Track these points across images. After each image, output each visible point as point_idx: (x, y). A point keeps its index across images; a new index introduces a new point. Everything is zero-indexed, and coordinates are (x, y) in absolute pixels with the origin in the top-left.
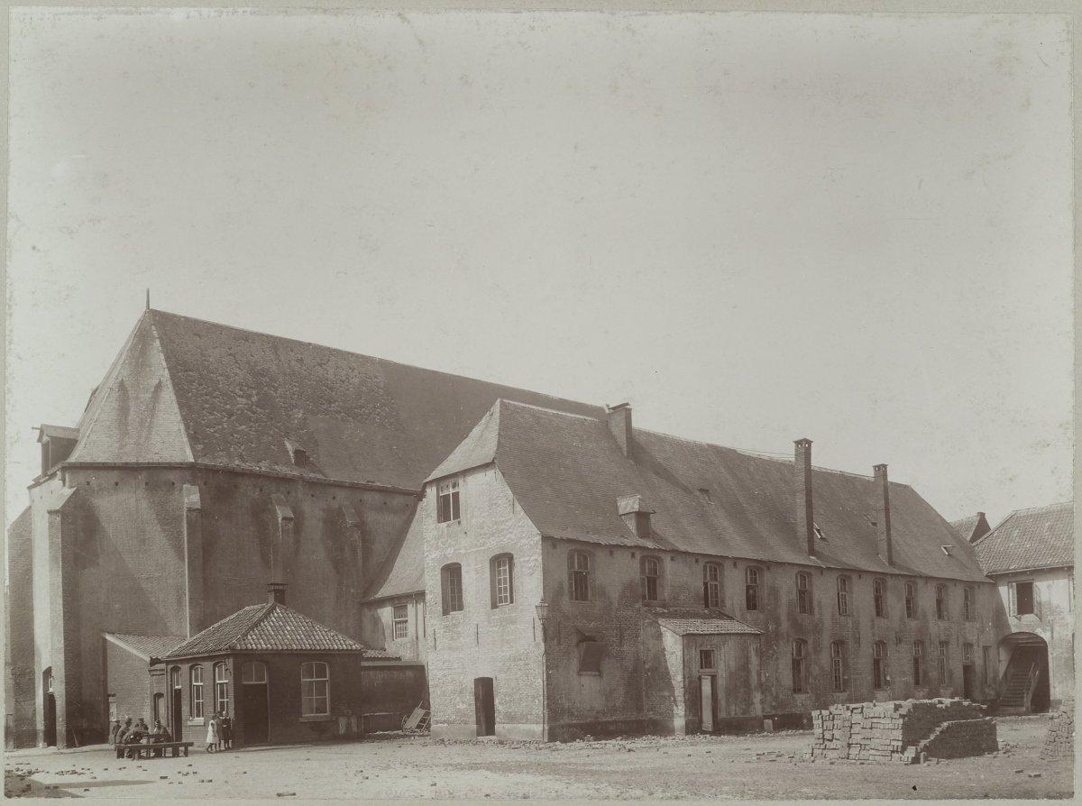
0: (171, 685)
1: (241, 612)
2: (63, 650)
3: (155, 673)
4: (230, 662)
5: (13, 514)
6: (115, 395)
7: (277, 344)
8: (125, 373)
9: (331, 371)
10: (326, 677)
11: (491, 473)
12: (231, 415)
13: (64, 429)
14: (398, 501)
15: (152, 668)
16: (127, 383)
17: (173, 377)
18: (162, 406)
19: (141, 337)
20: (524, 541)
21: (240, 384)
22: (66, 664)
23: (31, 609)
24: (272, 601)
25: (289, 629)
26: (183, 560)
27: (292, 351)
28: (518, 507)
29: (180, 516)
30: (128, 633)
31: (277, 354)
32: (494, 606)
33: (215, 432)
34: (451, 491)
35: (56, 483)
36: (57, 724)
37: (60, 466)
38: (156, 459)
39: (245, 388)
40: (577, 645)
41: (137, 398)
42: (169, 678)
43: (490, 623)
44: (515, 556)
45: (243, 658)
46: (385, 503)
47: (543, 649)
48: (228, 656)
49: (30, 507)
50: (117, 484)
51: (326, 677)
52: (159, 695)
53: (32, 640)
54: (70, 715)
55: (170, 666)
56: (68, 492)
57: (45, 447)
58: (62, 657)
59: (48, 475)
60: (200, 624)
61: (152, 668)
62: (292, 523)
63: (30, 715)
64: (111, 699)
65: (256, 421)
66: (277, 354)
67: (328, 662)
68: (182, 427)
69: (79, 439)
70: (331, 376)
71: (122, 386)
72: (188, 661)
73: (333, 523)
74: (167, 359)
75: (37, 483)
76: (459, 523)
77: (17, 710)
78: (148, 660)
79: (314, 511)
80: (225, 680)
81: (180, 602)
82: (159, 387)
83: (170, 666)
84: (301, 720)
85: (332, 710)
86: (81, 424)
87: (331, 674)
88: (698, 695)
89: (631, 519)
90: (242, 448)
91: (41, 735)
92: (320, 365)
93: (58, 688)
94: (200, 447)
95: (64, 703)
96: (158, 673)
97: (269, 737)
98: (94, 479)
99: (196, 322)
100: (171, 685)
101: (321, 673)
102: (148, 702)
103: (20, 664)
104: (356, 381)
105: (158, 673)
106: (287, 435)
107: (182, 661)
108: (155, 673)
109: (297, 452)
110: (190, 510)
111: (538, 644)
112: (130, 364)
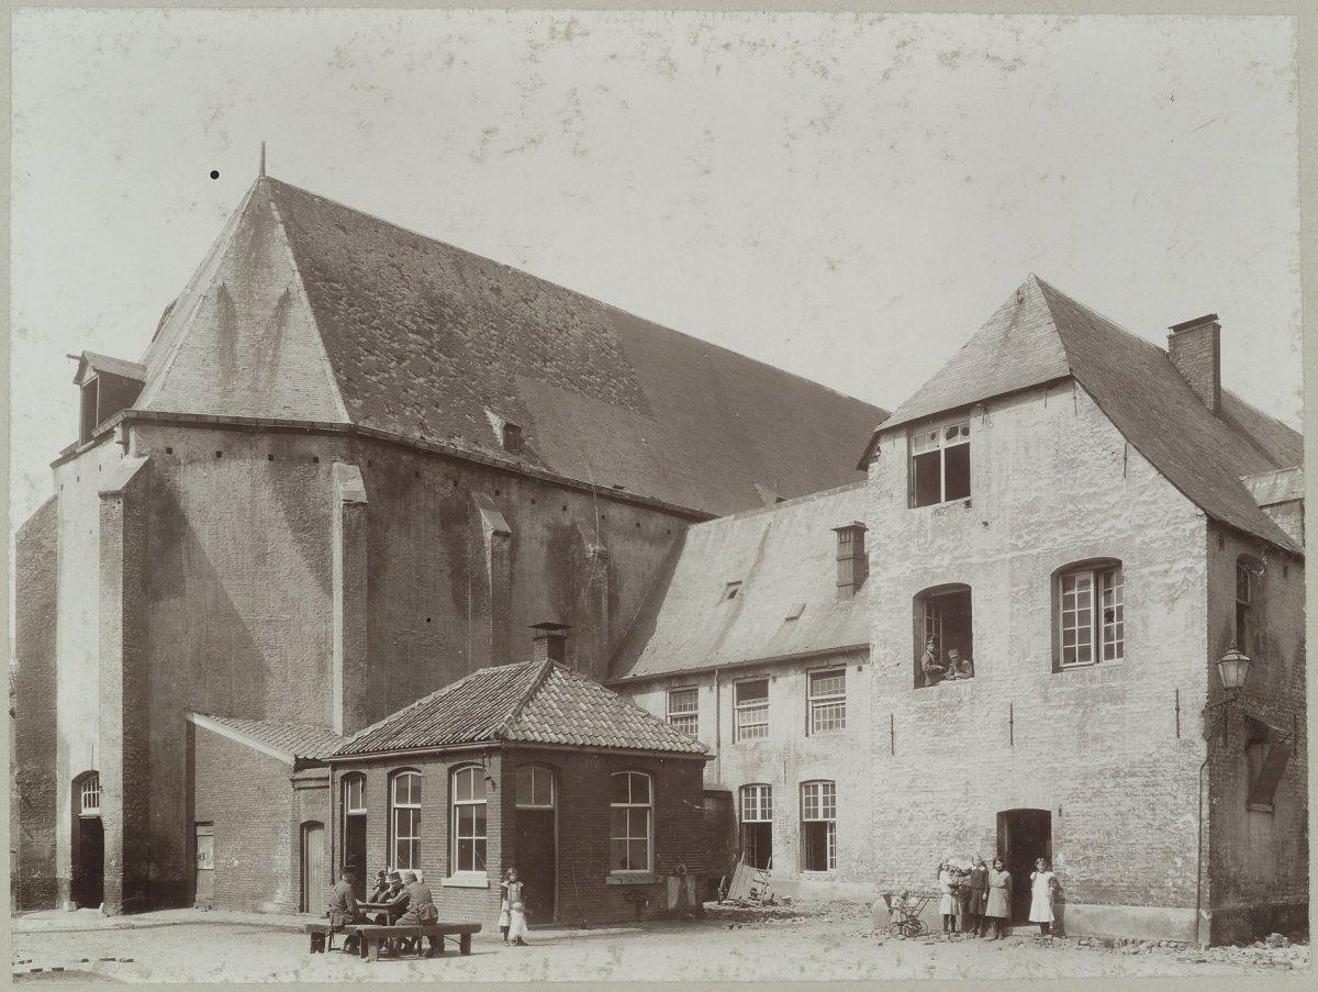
0: (342, 807)
1: (471, 677)
2: (120, 740)
3: (302, 784)
4: (494, 767)
5: (21, 514)
6: (211, 309)
7: (461, 261)
8: (228, 273)
9: (541, 314)
10: (647, 802)
11: (1060, 401)
12: (401, 359)
13: (123, 363)
14: (657, 522)
15: (298, 776)
16: (231, 289)
17: (308, 287)
18: (291, 331)
19: (254, 218)
20: (1151, 533)
21: (412, 312)
22: (125, 766)
23: (52, 671)
24: (541, 663)
25: (585, 707)
26: (327, 588)
27: (483, 273)
28: (1139, 463)
29: (328, 517)
30: (230, 716)
31: (461, 276)
32: (1056, 669)
33: (379, 382)
34: (943, 444)
35: (112, 448)
36: (106, 870)
37: (120, 417)
38: (286, 415)
39: (420, 320)
40: (1247, 749)
41: (250, 316)
42: (338, 793)
43: (1047, 699)
44: (1125, 564)
45: (521, 757)
46: (638, 525)
47: (1204, 754)
48: (490, 751)
49: (56, 498)
50: (219, 454)
51: (647, 802)
52: (313, 825)
53: (53, 725)
54: (130, 854)
55: (341, 773)
56: (134, 464)
57: (89, 392)
58: (118, 753)
59: (92, 433)
60: (365, 708)
61: (298, 776)
62: (508, 542)
63: (47, 853)
64: (201, 831)
65: (441, 373)
66: (461, 276)
67: (653, 774)
68: (328, 367)
69: (148, 380)
70: (541, 319)
71: (223, 293)
72: (384, 762)
73: (563, 544)
74: (297, 257)
75: (70, 455)
76: (968, 504)
77: (25, 845)
78: (291, 761)
79: (535, 530)
80: (487, 799)
81: (323, 667)
82: (286, 300)
83: (341, 773)
84: (609, 881)
85: (657, 865)
86: (150, 358)
87: (656, 796)
88: (1293, 848)
89: (1288, 513)
90: (423, 412)
91: (66, 887)
92: (526, 301)
93: (110, 810)
94: (358, 403)
95: (120, 835)
96: (313, 784)
97: (556, 912)
98: (182, 442)
99: (338, 208)
100: (342, 807)
101: (641, 795)
102: (287, 836)
103: (30, 766)
104: (577, 332)
105: (313, 784)
106: (487, 401)
107: (370, 763)
108: (302, 784)
109: (508, 427)
110: (349, 504)
111: (1188, 745)
112: (236, 260)
